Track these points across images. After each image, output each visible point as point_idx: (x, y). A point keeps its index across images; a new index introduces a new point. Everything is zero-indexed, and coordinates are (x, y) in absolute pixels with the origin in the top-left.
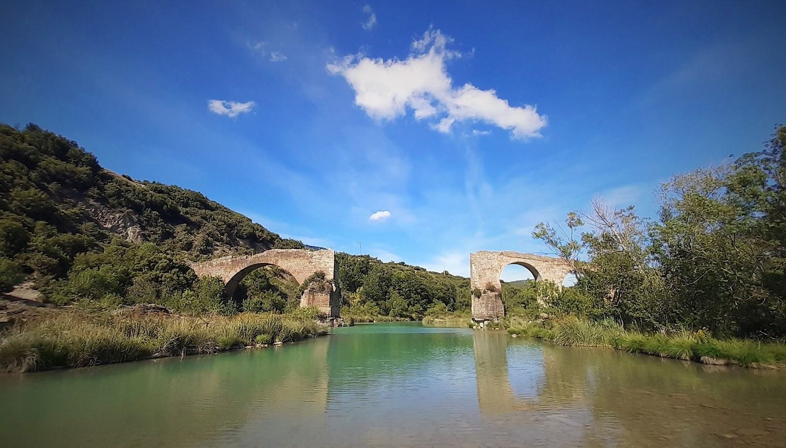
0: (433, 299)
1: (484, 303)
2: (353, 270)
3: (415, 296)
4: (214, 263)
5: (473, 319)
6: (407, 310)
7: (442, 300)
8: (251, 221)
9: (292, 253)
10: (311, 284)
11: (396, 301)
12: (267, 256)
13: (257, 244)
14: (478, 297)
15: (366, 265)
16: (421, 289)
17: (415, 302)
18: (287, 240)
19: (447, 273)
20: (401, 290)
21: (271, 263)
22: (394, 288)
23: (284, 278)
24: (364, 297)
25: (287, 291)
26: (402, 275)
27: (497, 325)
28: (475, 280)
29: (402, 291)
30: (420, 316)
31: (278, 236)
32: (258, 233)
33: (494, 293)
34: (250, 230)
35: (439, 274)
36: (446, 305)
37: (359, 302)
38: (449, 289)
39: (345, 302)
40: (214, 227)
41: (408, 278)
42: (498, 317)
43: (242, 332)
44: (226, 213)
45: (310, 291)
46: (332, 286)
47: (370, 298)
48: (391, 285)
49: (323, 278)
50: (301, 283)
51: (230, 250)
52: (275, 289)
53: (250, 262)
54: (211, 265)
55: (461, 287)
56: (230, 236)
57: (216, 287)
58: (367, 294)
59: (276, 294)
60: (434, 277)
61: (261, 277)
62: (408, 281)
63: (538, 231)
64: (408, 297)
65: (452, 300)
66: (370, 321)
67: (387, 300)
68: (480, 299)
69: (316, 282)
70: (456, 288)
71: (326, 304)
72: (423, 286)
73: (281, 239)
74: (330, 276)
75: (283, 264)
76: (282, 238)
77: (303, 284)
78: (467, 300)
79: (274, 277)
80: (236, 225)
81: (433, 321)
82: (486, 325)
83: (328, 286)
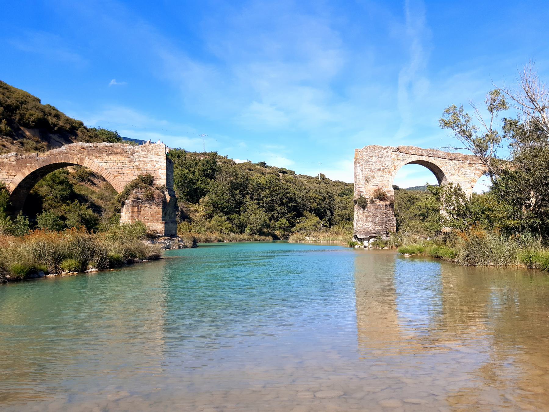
0: (303, 211)
1: (370, 216)
2: (194, 172)
5: (356, 237)
6: (268, 226)
7: (315, 213)
8: (39, 101)
9: (103, 148)
11: (255, 214)
12: (67, 153)
13: (51, 135)
15: (212, 166)
16: (287, 198)
17: (280, 215)
19: (322, 177)
20: (262, 200)
22: (251, 198)
23: (95, 184)
24: (210, 210)
25: (100, 203)
27: (386, 243)
28: (360, 186)
29: (262, 202)
30: (286, 233)
31: (81, 124)
32: (52, 120)
34: (38, 115)
35: (313, 178)
36: (321, 219)
37: (203, 216)
39: (185, 217)
41: (270, 183)
42: (387, 233)
45: (133, 201)
46: (165, 195)
47: (219, 211)
48: (247, 193)
50: (120, 190)
51: (13, 143)
52: (82, 199)
55: (341, 195)
56: (10, 123)
58: (215, 205)
59: (84, 207)
60: (305, 182)
61: (61, 183)
62: (270, 188)
63: (448, 118)
64: (271, 209)
65: (328, 213)
66: (220, 241)
68: (365, 211)
69: (141, 189)
71: (157, 220)
72: (290, 195)
74: (161, 180)
75: (92, 164)
78: (348, 212)
80: (17, 107)
81: (303, 240)
83: (159, 195)
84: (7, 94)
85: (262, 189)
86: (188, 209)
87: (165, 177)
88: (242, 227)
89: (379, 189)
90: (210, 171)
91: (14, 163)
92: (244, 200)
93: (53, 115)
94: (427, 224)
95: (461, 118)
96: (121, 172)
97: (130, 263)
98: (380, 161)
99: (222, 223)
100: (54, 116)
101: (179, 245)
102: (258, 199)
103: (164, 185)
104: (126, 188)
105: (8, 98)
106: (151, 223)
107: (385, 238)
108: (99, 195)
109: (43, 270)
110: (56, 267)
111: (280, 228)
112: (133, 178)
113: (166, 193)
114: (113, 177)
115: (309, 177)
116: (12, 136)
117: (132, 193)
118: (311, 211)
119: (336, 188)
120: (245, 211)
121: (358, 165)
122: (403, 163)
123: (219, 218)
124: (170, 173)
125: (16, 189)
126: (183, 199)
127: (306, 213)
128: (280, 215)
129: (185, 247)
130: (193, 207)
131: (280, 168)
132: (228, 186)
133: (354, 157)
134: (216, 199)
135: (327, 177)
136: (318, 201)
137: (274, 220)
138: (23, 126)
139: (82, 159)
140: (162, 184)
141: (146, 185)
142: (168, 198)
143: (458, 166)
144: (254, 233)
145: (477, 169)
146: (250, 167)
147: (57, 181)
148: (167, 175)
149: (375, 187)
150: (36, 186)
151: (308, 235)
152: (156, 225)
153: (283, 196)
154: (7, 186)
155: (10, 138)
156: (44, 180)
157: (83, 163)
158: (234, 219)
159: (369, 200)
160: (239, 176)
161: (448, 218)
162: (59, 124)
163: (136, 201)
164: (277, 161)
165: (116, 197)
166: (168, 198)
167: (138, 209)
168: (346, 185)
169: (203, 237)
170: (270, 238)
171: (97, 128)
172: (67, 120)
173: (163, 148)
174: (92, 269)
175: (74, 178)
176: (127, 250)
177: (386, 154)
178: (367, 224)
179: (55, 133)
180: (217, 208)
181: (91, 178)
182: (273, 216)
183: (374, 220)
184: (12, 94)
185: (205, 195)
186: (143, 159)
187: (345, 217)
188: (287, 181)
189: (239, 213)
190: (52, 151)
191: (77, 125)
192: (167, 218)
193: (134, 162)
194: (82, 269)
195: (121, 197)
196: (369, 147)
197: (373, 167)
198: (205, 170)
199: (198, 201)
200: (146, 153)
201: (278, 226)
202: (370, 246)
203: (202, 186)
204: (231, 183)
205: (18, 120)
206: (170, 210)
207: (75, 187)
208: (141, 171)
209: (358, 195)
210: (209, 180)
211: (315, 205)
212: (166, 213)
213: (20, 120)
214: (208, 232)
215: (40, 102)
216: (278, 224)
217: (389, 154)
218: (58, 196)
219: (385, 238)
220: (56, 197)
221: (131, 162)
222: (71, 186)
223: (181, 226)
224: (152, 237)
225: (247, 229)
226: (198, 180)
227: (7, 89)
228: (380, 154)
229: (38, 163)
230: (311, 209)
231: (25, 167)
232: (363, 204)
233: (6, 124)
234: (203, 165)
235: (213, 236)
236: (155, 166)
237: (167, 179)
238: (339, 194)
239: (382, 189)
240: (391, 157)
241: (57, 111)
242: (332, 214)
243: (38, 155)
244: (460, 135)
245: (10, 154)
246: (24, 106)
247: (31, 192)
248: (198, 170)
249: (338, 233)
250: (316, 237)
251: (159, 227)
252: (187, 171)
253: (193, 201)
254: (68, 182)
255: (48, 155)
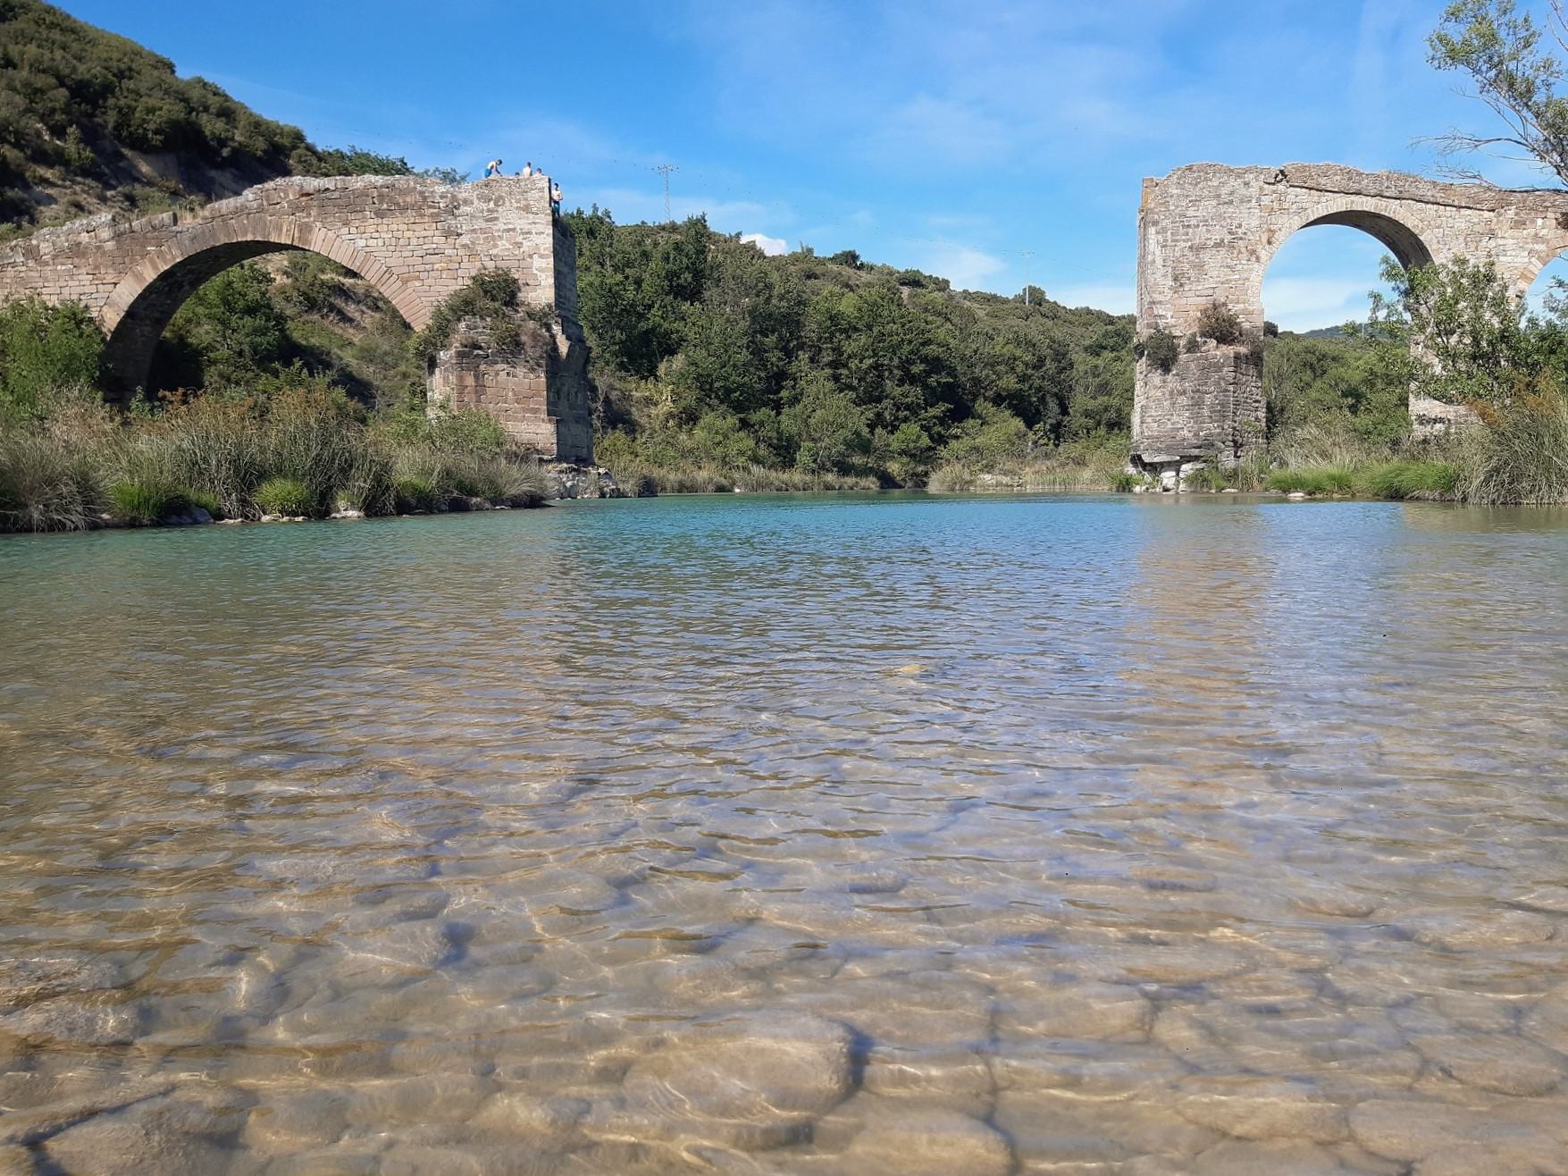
0: (974, 401)
1: (1184, 392)
2: (638, 283)
3: (899, 390)
4: (45, 248)
5: (1137, 460)
6: (865, 447)
7: (1010, 406)
8: (171, 67)
9: (364, 193)
10: (462, 325)
11: (824, 409)
12: (261, 210)
13: (213, 173)
14: (1162, 365)
15: (692, 261)
16: (924, 360)
17: (902, 414)
18: (343, 156)
19: (1036, 297)
20: (845, 366)
21: (285, 240)
22: (812, 360)
23: (351, 320)
24: (690, 398)
25: (368, 372)
26: (847, 305)
27: (1232, 476)
28: (1157, 297)
29: (845, 372)
30: (920, 469)
31: (299, 137)
32: (211, 126)
33: (1229, 350)
34: (171, 109)
35: (1006, 301)
36: (1030, 425)
37: (671, 415)
38: (1041, 361)
39: (618, 418)
40: (18, 99)
41: (872, 314)
42: (1237, 446)
43: (196, 469)
44: (56, 35)
45: (460, 355)
46: (553, 337)
47: (716, 402)
48: (801, 347)
49: (511, 300)
50: (421, 322)
51: (103, 200)
52: (316, 360)
53: (193, 239)
54: (32, 253)
55: (1096, 350)
56: (90, 136)
57: (62, 342)
58: (705, 385)
59: (321, 380)
60: (981, 313)
61: (251, 311)
62: (870, 327)
63: (1457, 33)
64: (872, 396)
65: (1053, 405)
66: (721, 489)
67: (786, 410)
68: (1169, 377)
69: (482, 318)
70: (1074, 357)
71: (535, 411)
72: (932, 350)
73: (315, 153)
74: (540, 291)
75: (336, 242)
76: (319, 149)
77: (428, 327)
78: (1116, 402)
79: (306, 317)
80: (107, 89)
81: (970, 482)
82: (1187, 480)
83: (535, 336)
84: (75, 46)
85: (845, 331)
86: (626, 397)
87: (552, 281)
88: (787, 448)
89: (1215, 307)
90: (688, 276)
91: (110, 245)
92: (793, 369)
93: (213, 110)
94: (1363, 420)
95: (1502, 34)
96: (421, 268)
97: (459, 507)
98: (1221, 217)
99: (726, 437)
100: (219, 115)
101: (601, 489)
102: (834, 365)
103: (549, 306)
104: (438, 314)
105: (80, 59)
106: (516, 419)
107: (1228, 461)
108: (362, 349)
109: (205, 507)
110: (244, 502)
111: (903, 453)
112: (455, 286)
113: (557, 329)
114: (399, 283)
115: (995, 296)
116: (98, 177)
117: (455, 331)
118: (998, 400)
119: (1079, 331)
120: (795, 400)
121: (1152, 230)
122: (1298, 221)
123: (717, 420)
124: (565, 270)
125: (120, 323)
126: (607, 363)
127: (982, 406)
128: (902, 414)
129: (619, 494)
130: (640, 390)
131: (902, 270)
132: (744, 324)
133: (1139, 206)
134: (709, 364)
135: (1050, 297)
136: (1020, 368)
137: (885, 427)
138: (132, 147)
139: (305, 229)
140: (544, 302)
141: (497, 305)
142: (563, 346)
143: (1477, 228)
144: (823, 467)
145: (1537, 238)
146: (807, 267)
147: (241, 304)
148: (558, 275)
149: (1202, 300)
150: (180, 315)
151: (989, 468)
152: (532, 428)
153: (911, 352)
154: (94, 315)
155: (93, 184)
156: (201, 300)
157: (307, 242)
158: (762, 424)
159: (1182, 342)
160: (775, 292)
161: (1438, 370)
162: (233, 139)
163: (470, 354)
164: (891, 252)
165: (412, 343)
166: (563, 346)
167: (476, 377)
168: (1111, 323)
169: (672, 477)
170: (872, 483)
171: (346, 150)
172: (257, 125)
173: (541, 190)
174: (347, 511)
175: (287, 299)
176: (448, 473)
177: (1243, 191)
178: (1175, 418)
179: (223, 165)
180: (713, 388)
181: (339, 302)
182: (879, 415)
183: (1198, 404)
184: (88, 47)
185: (673, 352)
186: (484, 225)
187: (1105, 416)
188: (926, 310)
189: (778, 407)
190: (216, 205)
191: (286, 142)
192: (563, 406)
193: (459, 235)
194: (319, 509)
195: (427, 342)
196: (1190, 168)
197: (1200, 235)
198: (672, 275)
199: (652, 371)
200: (492, 205)
201: (895, 446)
202: (1182, 486)
203: (666, 325)
204: (750, 313)
205: (115, 128)
206: (569, 383)
207: (290, 325)
208: (478, 264)
209: (1149, 326)
210: (686, 306)
211: (1009, 382)
212: (558, 393)
213: (118, 127)
214: (686, 464)
215: (173, 72)
216: (896, 440)
217: (1254, 191)
218: (246, 348)
219: (1228, 461)
220: (240, 354)
221: (448, 234)
222: (281, 319)
223: (606, 443)
224: (526, 455)
225: (802, 457)
226: (650, 307)
227: (73, 31)
228: (1224, 191)
229: (180, 245)
230: (999, 395)
231: (143, 257)
232: (1162, 353)
233: (81, 141)
234: (667, 259)
235: (702, 475)
236: (519, 245)
237: (558, 286)
238: (1086, 349)
239: (1224, 304)
240: (1259, 200)
241: (226, 98)
242: (1064, 411)
243: (175, 220)
244: (1494, 94)
245: (96, 218)
246: (125, 83)
247: (167, 334)
248: (652, 273)
249: (1081, 462)
250: (1012, 473)
251: (542, 433)
252: (619, 277)
253: (637, 372)
254: (268, 306)
255: (204, 218)
